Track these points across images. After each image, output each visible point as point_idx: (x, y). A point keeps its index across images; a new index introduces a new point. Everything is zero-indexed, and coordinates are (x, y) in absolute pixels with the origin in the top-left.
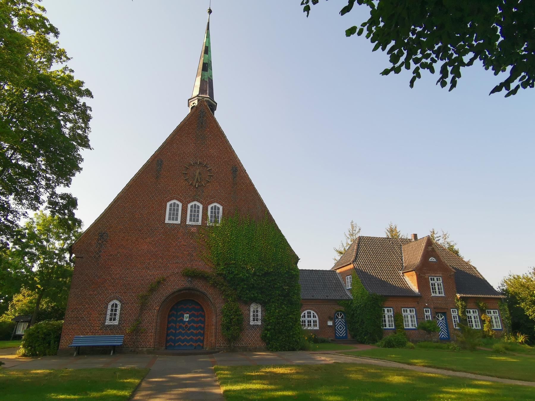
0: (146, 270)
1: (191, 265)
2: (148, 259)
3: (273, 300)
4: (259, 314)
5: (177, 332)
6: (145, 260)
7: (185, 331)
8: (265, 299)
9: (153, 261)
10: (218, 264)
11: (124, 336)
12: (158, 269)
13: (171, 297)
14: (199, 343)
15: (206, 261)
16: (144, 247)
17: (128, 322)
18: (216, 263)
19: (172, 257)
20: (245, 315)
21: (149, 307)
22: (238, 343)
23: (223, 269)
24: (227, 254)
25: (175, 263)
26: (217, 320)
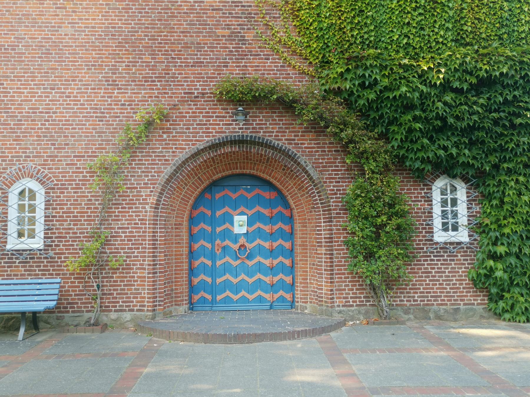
0: (108, 89)
1: (243, 70)
2: (110, 54)
3: (511, 166)
4: (462, 209)
5: (219, 263)
6: (101, 58)
7: (239, 262)
8: (482, 163)
9: (124, 62)
10: (325, 63)
11: (58, 280)
12: (144, 85)
13: (189, 166)
14: (281, 293)
15: (285, 54)
16: (94, 19)
17: (73, 241)
18: (318, 58)
19: (182, 47)
20: (416, 213)
21: (129, 196)
22: (399, 297)
23: (342, 74)
24: (352, 30)
25: (192, 66)
26: (331, 230)
